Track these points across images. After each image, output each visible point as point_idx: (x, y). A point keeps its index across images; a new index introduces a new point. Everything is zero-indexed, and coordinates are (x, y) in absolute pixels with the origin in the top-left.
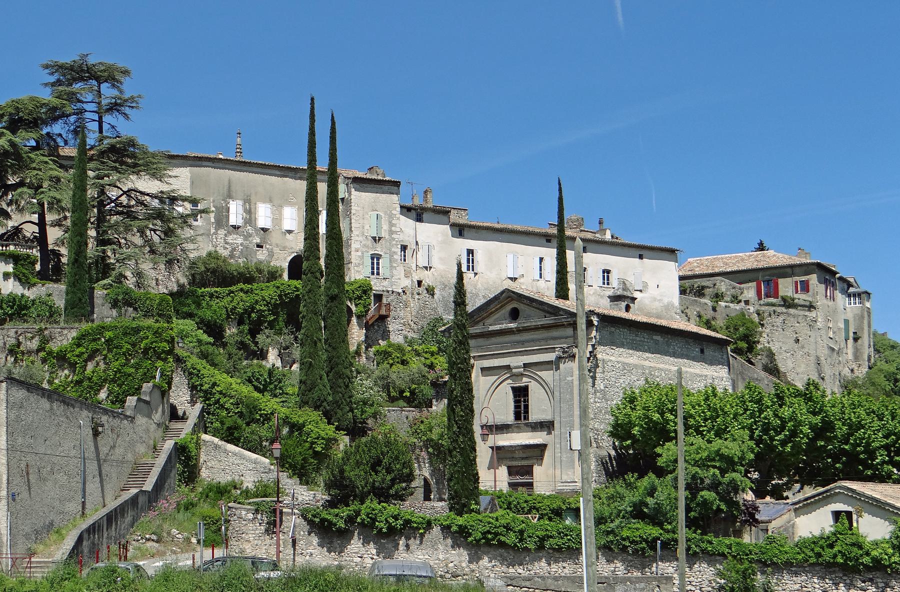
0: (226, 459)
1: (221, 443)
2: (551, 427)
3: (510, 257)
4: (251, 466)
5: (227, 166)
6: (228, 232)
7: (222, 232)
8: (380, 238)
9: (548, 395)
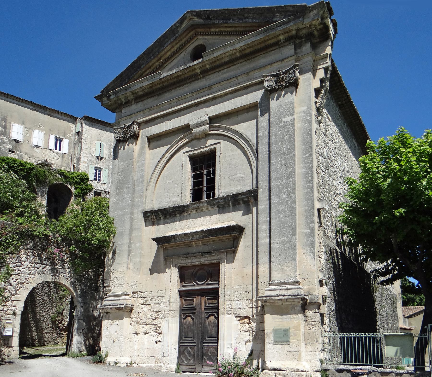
2: (252, 201)
8: (102, 158)
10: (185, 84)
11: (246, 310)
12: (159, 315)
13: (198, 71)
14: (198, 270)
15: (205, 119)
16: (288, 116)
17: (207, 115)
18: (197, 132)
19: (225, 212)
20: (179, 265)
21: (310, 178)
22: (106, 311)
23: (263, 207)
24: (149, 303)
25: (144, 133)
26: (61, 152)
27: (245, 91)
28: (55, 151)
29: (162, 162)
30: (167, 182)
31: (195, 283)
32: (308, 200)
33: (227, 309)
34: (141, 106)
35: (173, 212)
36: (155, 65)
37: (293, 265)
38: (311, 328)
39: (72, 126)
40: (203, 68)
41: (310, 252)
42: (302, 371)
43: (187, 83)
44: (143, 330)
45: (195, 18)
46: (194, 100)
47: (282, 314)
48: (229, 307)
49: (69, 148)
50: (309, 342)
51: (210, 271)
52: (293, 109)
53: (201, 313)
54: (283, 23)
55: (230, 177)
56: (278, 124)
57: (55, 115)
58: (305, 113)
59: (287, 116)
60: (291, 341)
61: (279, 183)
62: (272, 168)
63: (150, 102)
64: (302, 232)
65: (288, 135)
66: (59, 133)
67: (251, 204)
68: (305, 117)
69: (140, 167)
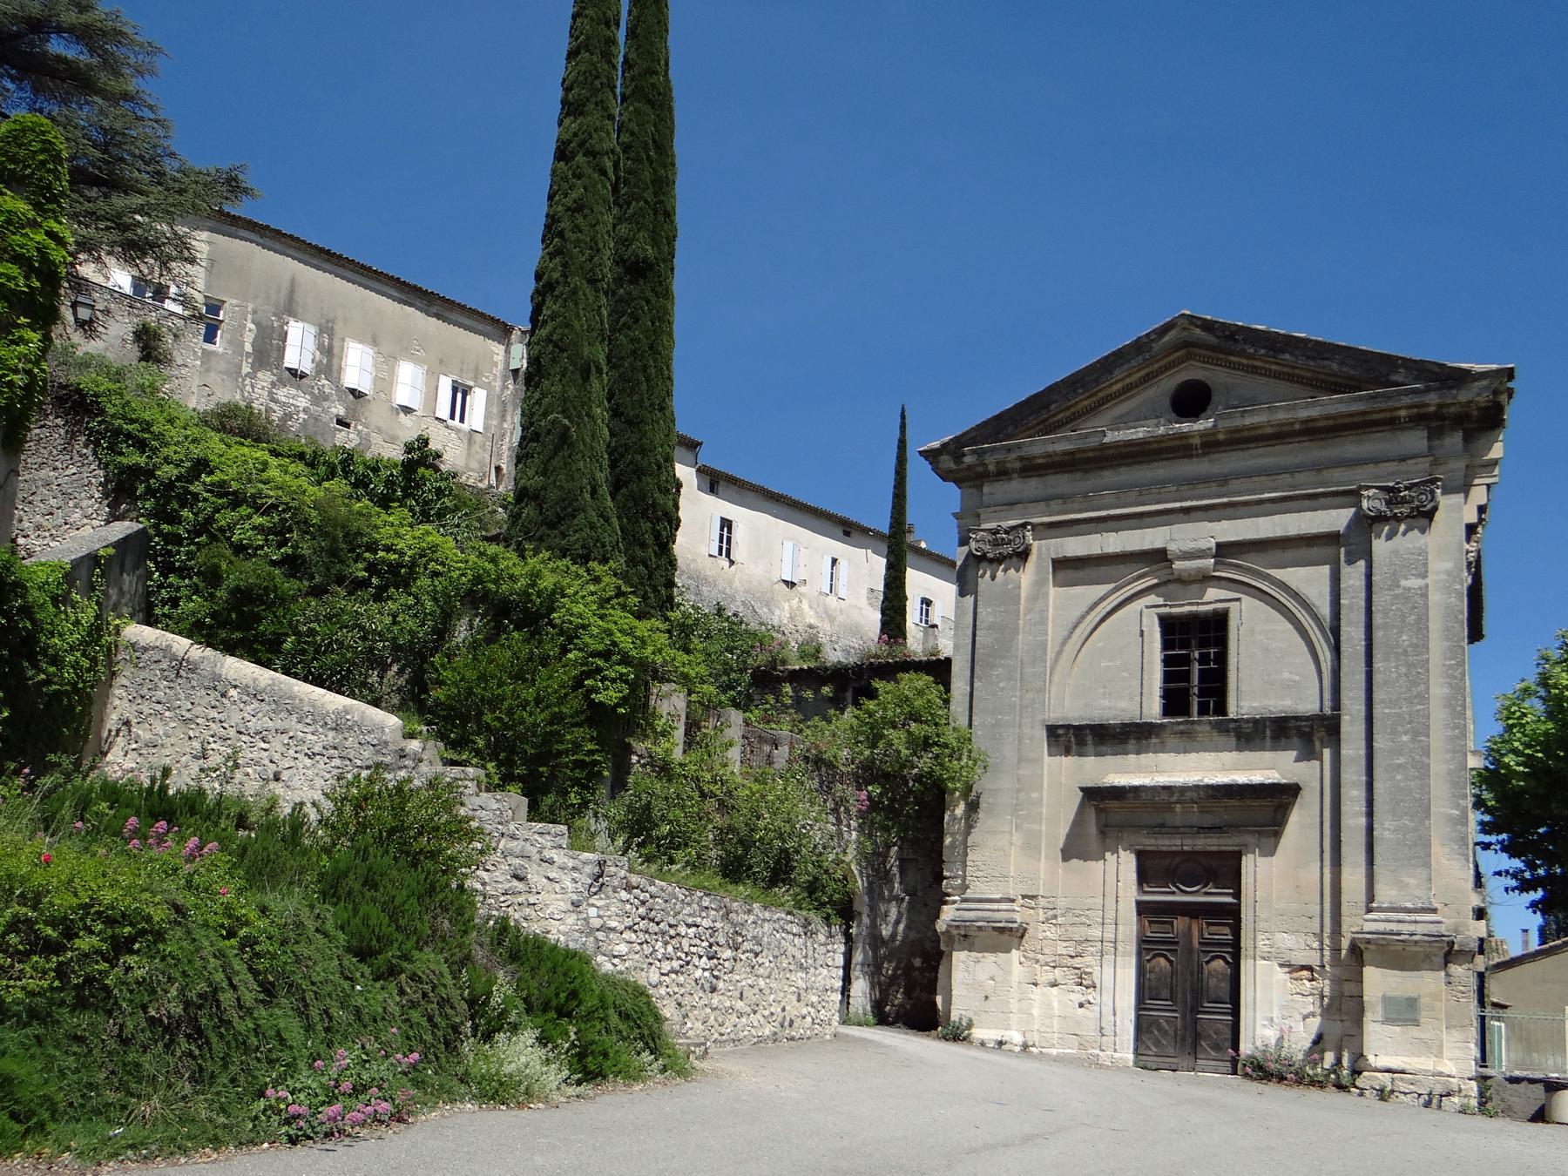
0: (213, 713)
1: (197, 652)
3: (789, 545)
4: (316, 741)
5: (290, 251)
6: (280, 380)
7: (265, 378)
11: (1304, 953)
13: (1196, 441)
15: (1209, 545)
18: (1184, 570)
21: (1459, 708)
22: (963, 933)
23: (1351, 752)
24: (1060, 920)
26: (465, 427)
27: (1307, 503)
28: (450, 422)
29: (1089, 618)
31: (1174, 889)
36: (1079, 407)
37: (1425, 876)
39: (498, 349)
42: (1449, 1076)
43: (1163, 460)
44: (1050, 977)
49: (487, 416)
52: (1426, 565)
53: (1190, 950)
54: (1415, 392)
57: (455, 316)
60: (1422, 1020)
63: (1061, 483)
66: (462, 370)
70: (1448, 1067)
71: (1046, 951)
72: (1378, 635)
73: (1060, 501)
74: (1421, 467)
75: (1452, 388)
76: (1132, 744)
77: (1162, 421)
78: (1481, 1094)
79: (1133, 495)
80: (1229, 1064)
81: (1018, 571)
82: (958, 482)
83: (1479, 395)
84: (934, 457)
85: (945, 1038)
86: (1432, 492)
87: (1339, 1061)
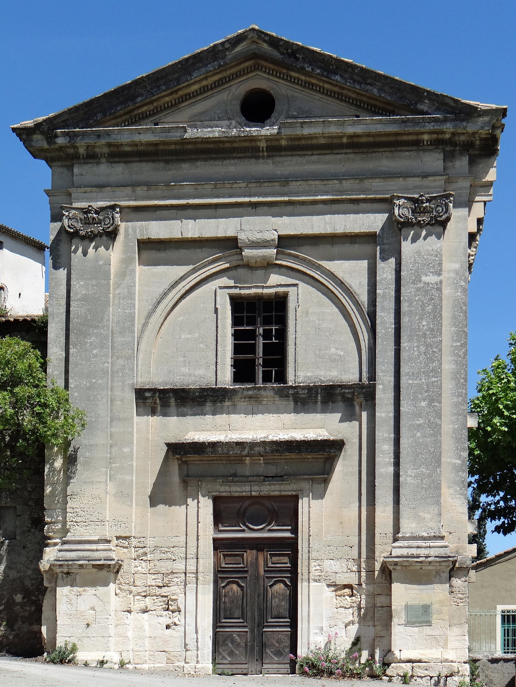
2: (359, 400)
9: (354, 313)
10: (229, 158)
11: (347, 575)
12: (174, 580)
13: (263, 144)
14: (250, 505)
16: (431, 274)
17: (276, 230)
18: (252, 257)
19: (307, 412)
20: (214, 494)
22: (65, 570)
23: (383, 415)
25: (130, 230)
27: (351, 206)
29: (171, 295)
30: (183, 337)
31: (244, 528)
32: (459, 415)
33: (314, 573)
34: (123, 174)
35: (200, 397)
36: (181, 93)
37: (436, 511)
38: (458, 603)
40: (274, 143)
41: (461, 494)
42: (452, 662)
43: (234, 158)
44: (142, 605)
45: (264, 44)
46: (250, 196)
47: (420, 583)
48: (315, 570)
50: (455, 623)
51: (276, 509)
52: (440, 264)
53: (257, 577)
55: (317, 352)
56: (413, 283)
58: (457, 274)
59: (429, 274)
60: (433, 622)
61: (415, 382)
62: (404, 355)
64: (448, 463)
65: (430, 307)
67: (356, 404)
68: (457, 281)
69: (123, 299)
70: (450, 655)
71: (137, 583)
72: (405, 320)
73: (145, 188)
74: (437, 184)
75: (463, 120)
76: (208, 406)
77: (234, 123)
78: (472, 673)
79: (208, 187)
80: (288, 666)
81: (107, 249)
82: (49, 161)
83: (482, 128)
84: (28, 135)
85: (53, 661)
86: (446, 205)
87: (372, 655)
